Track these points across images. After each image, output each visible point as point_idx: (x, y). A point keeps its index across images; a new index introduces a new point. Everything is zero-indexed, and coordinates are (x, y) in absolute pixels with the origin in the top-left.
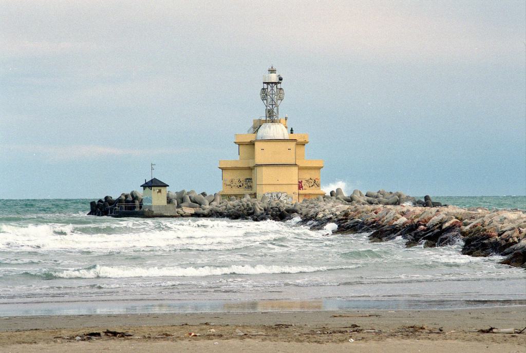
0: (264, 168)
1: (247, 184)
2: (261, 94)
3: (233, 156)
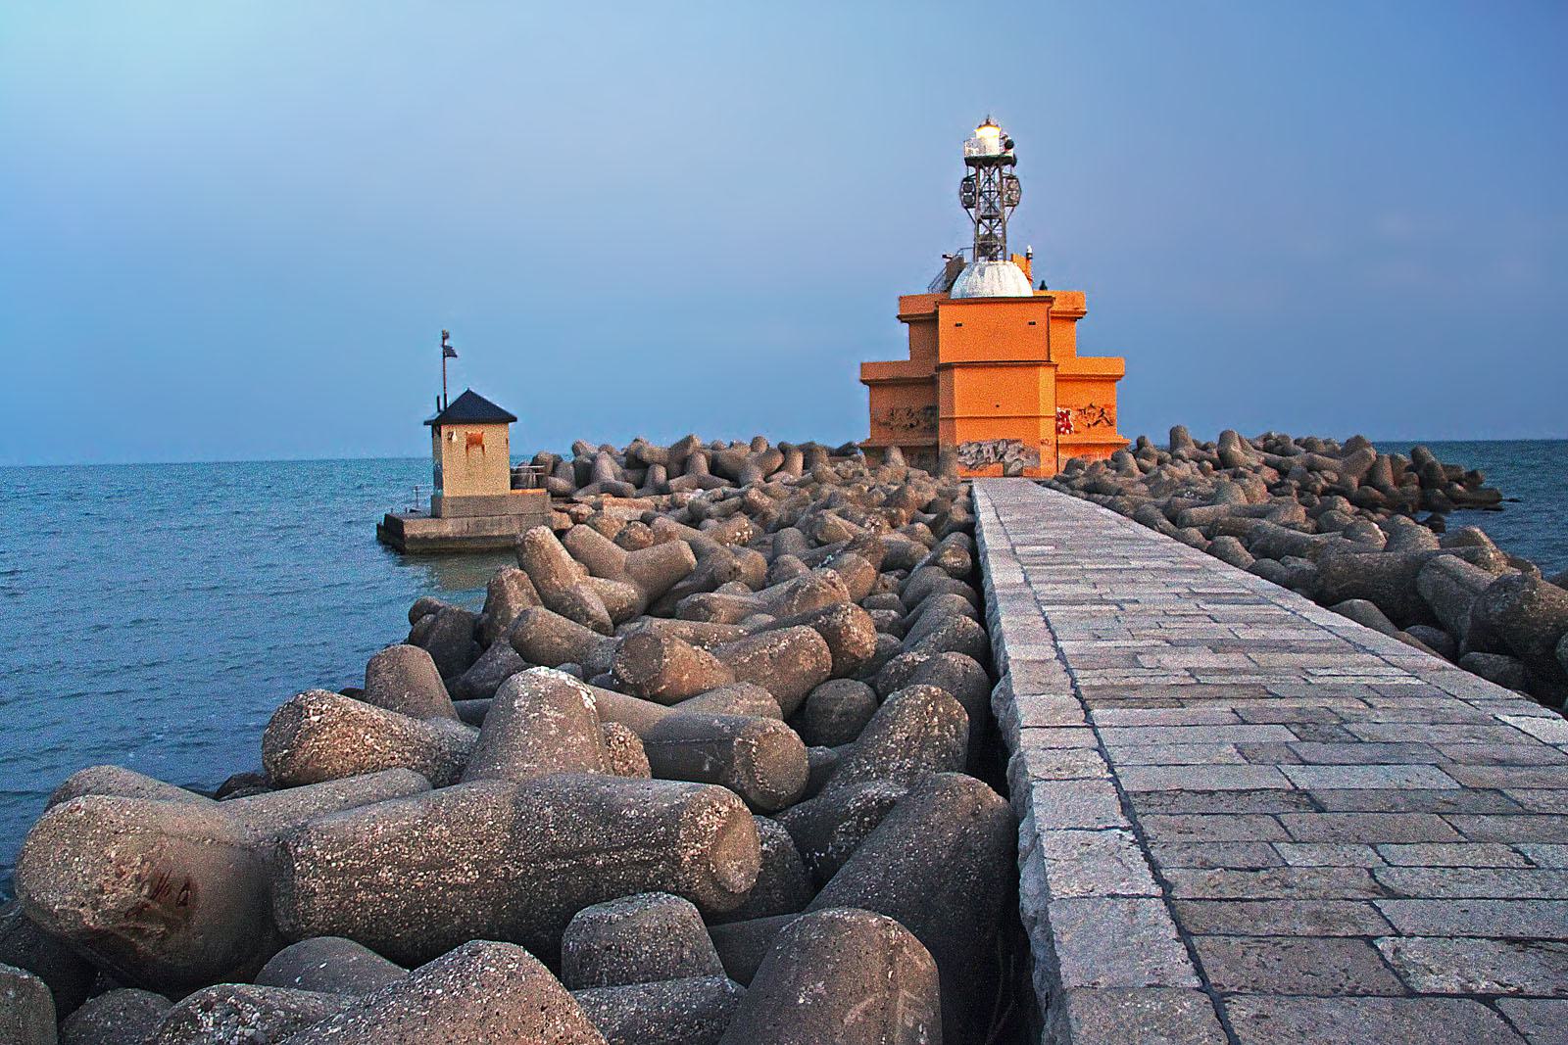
0: (957, 373)
1: (929, 420)
2: (961, 194)
3: (896, 346)
